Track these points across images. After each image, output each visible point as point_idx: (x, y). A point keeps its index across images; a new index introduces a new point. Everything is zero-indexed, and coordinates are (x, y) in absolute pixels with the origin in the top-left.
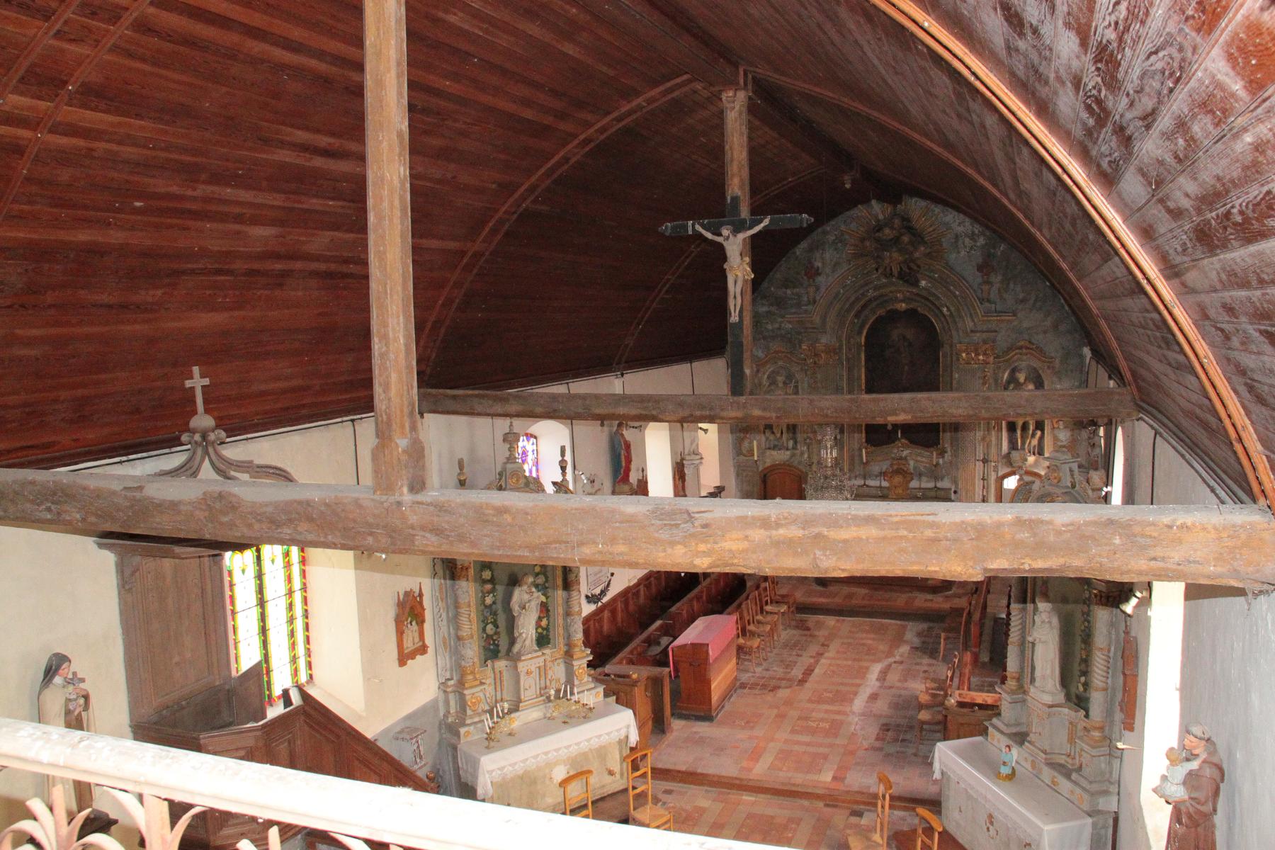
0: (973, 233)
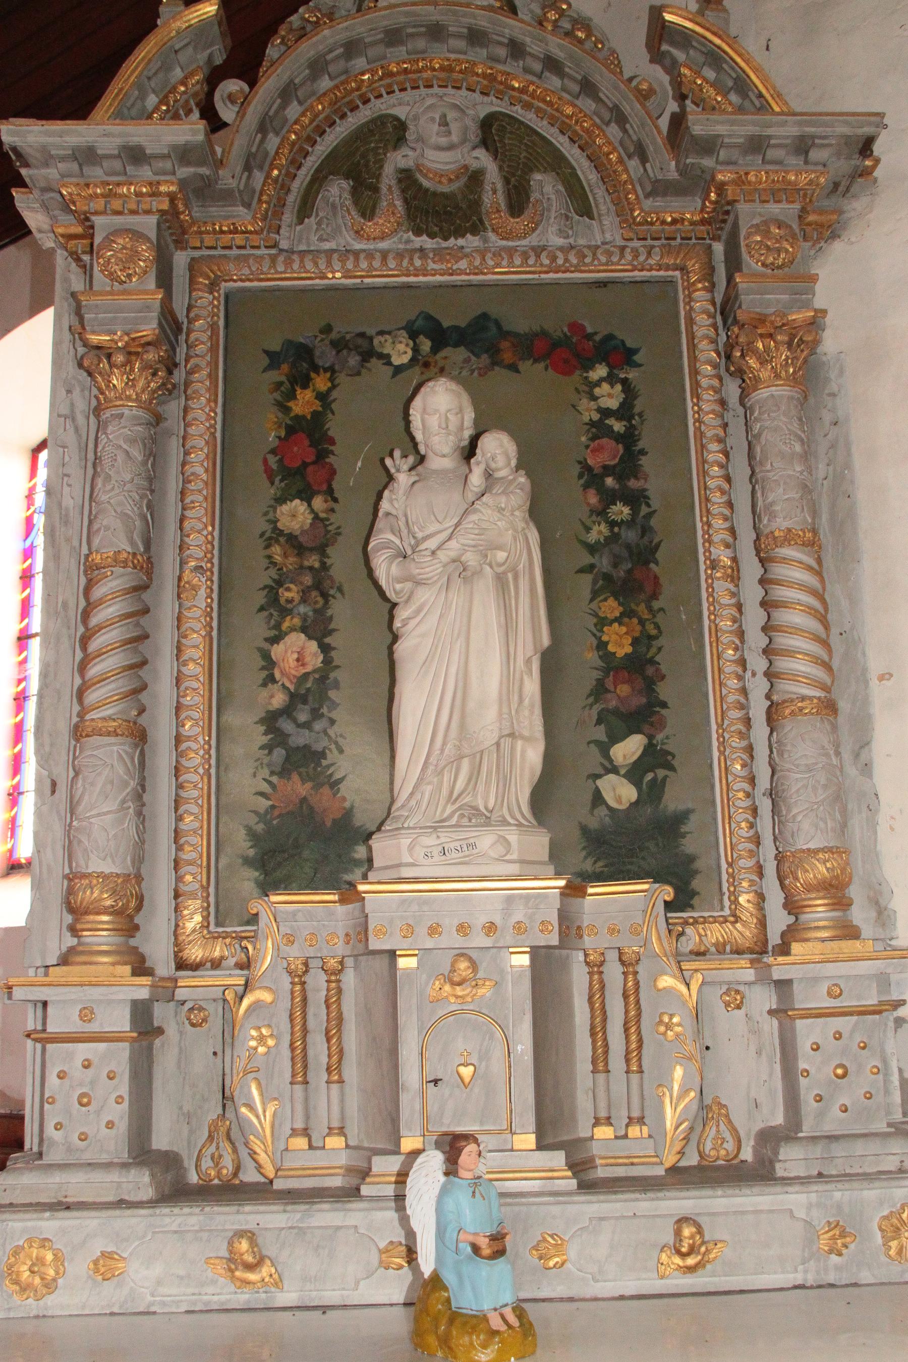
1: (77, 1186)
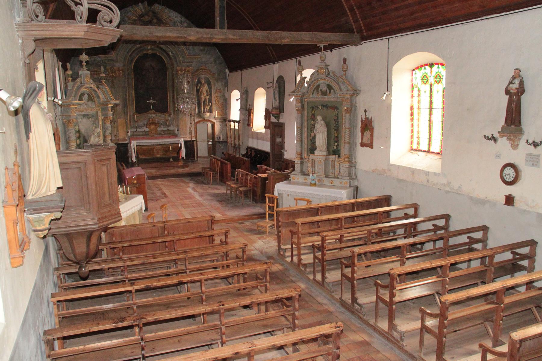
0: (181, 21)
1: (297, 173)
